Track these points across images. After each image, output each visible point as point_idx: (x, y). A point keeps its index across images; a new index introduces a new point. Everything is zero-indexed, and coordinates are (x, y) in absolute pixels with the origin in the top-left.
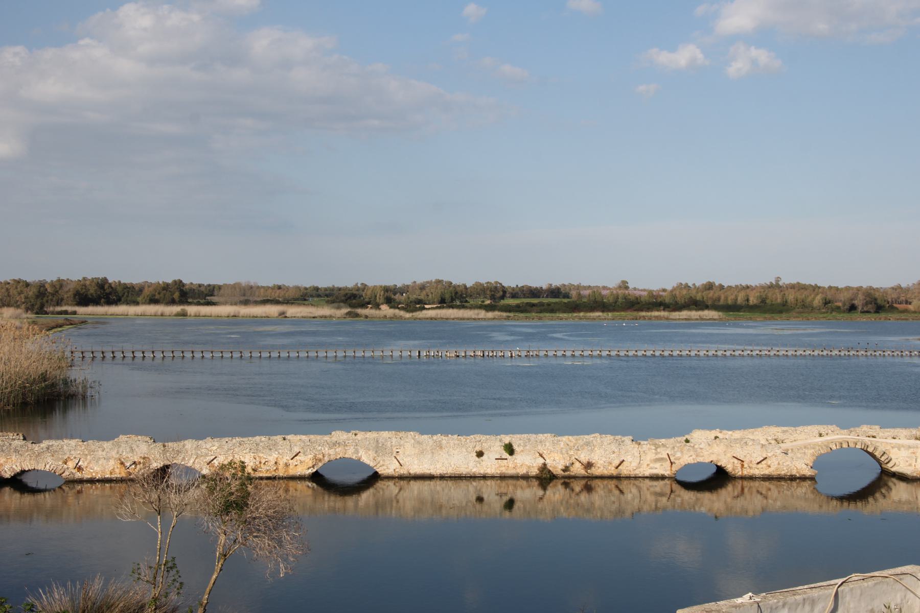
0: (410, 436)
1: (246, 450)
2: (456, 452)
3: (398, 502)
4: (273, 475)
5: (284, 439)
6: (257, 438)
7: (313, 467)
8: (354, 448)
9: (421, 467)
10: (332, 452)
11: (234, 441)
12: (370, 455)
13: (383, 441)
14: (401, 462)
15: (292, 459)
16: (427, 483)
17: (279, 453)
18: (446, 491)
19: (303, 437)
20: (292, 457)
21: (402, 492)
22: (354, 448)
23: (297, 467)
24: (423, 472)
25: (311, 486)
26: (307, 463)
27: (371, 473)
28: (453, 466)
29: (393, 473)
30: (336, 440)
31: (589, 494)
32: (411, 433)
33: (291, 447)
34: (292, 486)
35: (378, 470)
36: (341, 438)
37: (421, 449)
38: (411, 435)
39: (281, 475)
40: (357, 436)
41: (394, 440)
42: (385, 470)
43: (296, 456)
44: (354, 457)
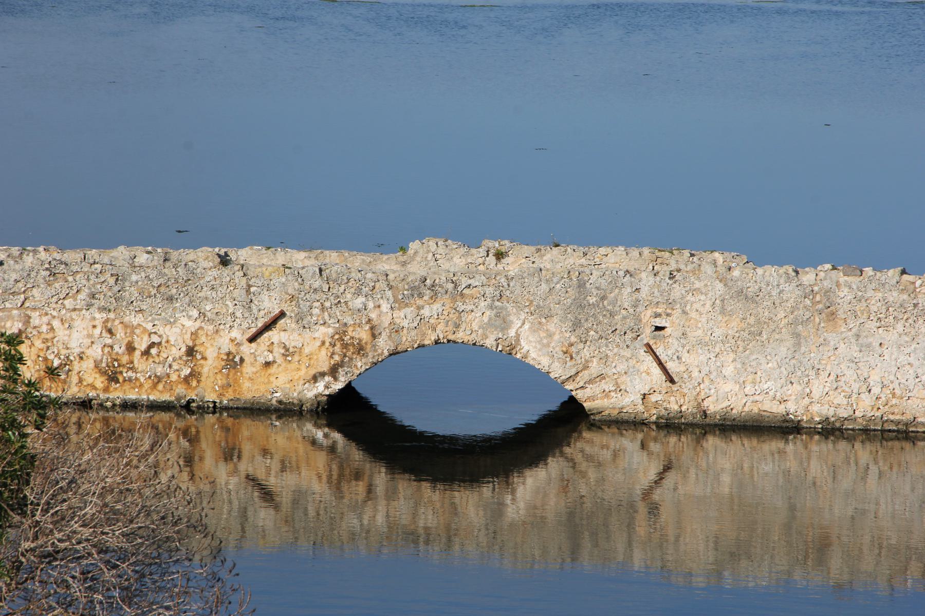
0: (708, 269)
1: (74, 298)
2: (891, 337)
3: (654, 510)
4: (179, 399)
5: (225, 261)
6: (121, 253)
7: (333, 371)
8: (491, 307)
9: (749, 389)
10: (405, 317)
11: (29, 259)
12: (550, 335)
13: (603, 283)
14: (671, 366)
15: (252, 339)
16: (775, 444)
17: (202, 314)
18: (846, 483)
19: (299, 258)
20: (254, 330)
21: (671, 478)
22: (491, 307)
23: (273, 369)
24: (756, 410)
25: (325, 442)
26: (310, 357)
27: (553, 405)
28: (876, 390)
29: (641, 408)
30: (422, 272)
31: (393, 479)
32: (716, 255)
33: (248, 291)
34: (250, 439)
35: (579, 395)
36: (445, 265)
37: (752, 320)
38: (715, 263)
39: (211, 397)
40: (505, 261)
41: (646, 281)
42: (606, 394)
43: (268, 327)
44: (490, 342)
